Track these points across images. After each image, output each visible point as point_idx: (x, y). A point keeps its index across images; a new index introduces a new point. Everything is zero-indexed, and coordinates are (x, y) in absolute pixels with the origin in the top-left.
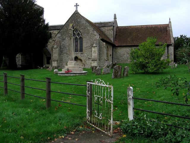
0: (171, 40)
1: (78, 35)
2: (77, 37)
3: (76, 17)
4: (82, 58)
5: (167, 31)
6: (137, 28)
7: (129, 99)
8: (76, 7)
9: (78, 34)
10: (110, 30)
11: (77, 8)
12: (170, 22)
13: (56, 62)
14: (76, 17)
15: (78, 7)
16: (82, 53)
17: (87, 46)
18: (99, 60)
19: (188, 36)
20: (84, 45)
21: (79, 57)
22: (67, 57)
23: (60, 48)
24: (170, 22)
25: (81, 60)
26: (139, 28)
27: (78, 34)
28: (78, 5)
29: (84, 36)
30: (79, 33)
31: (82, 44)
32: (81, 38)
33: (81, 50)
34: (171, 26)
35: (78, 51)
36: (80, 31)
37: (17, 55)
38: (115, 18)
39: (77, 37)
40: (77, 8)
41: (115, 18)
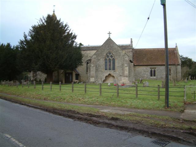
0: (178, 61)
1: (111, 57)
2: (111, 58)
3: (109, 42)
4: (114, 75)
5: (175, 53)
6: (150, 50)
7: (139, 97)
8: (109, 34)
9: (112, 56)
10: (130, 52)
11: (110, 35)
12: (176, 46)
13: (93, 78)
14: (109, 42)
15: (110, 34)
16: (114, 71)
17: (119, 65)
18: (129, 77)
19: (194, 60)
20: (117, 65)
21: (112, 74)
22: (102, 74)
23: (96, 67)
24: (176, 46)
25: (113, 77)
26: (152, 50)
27: (112, 56)
28: (111, 33)
29: (116, 57)
30: (112, 56)
31: (114, 64)
32: (114, 60)
33: (114, 69)
34: (177, 49)
35: (111, 70)
36: (113, 54)
37: (26, 43)
38: (132, 42)
39: (111, 58)
40: (110, 35)
41: (132, 42)
